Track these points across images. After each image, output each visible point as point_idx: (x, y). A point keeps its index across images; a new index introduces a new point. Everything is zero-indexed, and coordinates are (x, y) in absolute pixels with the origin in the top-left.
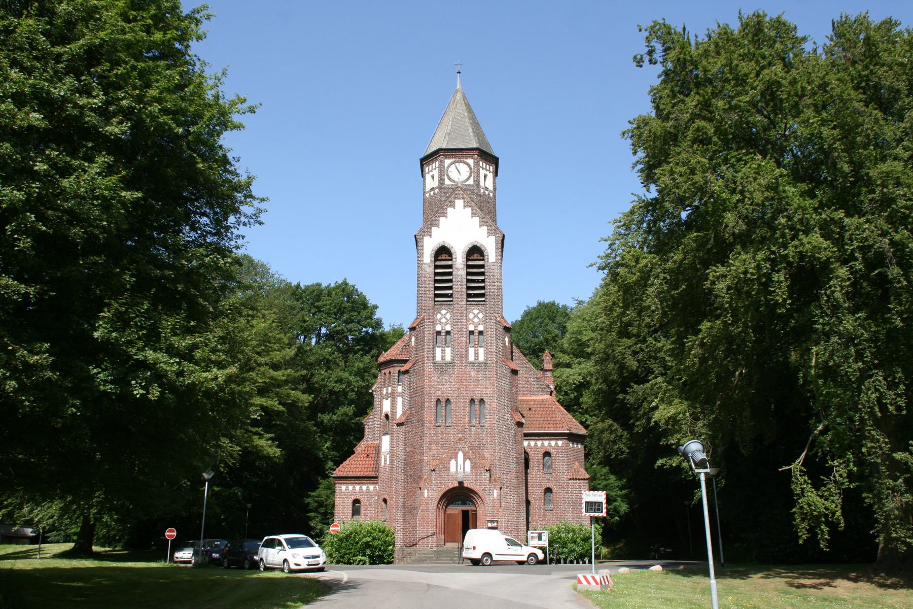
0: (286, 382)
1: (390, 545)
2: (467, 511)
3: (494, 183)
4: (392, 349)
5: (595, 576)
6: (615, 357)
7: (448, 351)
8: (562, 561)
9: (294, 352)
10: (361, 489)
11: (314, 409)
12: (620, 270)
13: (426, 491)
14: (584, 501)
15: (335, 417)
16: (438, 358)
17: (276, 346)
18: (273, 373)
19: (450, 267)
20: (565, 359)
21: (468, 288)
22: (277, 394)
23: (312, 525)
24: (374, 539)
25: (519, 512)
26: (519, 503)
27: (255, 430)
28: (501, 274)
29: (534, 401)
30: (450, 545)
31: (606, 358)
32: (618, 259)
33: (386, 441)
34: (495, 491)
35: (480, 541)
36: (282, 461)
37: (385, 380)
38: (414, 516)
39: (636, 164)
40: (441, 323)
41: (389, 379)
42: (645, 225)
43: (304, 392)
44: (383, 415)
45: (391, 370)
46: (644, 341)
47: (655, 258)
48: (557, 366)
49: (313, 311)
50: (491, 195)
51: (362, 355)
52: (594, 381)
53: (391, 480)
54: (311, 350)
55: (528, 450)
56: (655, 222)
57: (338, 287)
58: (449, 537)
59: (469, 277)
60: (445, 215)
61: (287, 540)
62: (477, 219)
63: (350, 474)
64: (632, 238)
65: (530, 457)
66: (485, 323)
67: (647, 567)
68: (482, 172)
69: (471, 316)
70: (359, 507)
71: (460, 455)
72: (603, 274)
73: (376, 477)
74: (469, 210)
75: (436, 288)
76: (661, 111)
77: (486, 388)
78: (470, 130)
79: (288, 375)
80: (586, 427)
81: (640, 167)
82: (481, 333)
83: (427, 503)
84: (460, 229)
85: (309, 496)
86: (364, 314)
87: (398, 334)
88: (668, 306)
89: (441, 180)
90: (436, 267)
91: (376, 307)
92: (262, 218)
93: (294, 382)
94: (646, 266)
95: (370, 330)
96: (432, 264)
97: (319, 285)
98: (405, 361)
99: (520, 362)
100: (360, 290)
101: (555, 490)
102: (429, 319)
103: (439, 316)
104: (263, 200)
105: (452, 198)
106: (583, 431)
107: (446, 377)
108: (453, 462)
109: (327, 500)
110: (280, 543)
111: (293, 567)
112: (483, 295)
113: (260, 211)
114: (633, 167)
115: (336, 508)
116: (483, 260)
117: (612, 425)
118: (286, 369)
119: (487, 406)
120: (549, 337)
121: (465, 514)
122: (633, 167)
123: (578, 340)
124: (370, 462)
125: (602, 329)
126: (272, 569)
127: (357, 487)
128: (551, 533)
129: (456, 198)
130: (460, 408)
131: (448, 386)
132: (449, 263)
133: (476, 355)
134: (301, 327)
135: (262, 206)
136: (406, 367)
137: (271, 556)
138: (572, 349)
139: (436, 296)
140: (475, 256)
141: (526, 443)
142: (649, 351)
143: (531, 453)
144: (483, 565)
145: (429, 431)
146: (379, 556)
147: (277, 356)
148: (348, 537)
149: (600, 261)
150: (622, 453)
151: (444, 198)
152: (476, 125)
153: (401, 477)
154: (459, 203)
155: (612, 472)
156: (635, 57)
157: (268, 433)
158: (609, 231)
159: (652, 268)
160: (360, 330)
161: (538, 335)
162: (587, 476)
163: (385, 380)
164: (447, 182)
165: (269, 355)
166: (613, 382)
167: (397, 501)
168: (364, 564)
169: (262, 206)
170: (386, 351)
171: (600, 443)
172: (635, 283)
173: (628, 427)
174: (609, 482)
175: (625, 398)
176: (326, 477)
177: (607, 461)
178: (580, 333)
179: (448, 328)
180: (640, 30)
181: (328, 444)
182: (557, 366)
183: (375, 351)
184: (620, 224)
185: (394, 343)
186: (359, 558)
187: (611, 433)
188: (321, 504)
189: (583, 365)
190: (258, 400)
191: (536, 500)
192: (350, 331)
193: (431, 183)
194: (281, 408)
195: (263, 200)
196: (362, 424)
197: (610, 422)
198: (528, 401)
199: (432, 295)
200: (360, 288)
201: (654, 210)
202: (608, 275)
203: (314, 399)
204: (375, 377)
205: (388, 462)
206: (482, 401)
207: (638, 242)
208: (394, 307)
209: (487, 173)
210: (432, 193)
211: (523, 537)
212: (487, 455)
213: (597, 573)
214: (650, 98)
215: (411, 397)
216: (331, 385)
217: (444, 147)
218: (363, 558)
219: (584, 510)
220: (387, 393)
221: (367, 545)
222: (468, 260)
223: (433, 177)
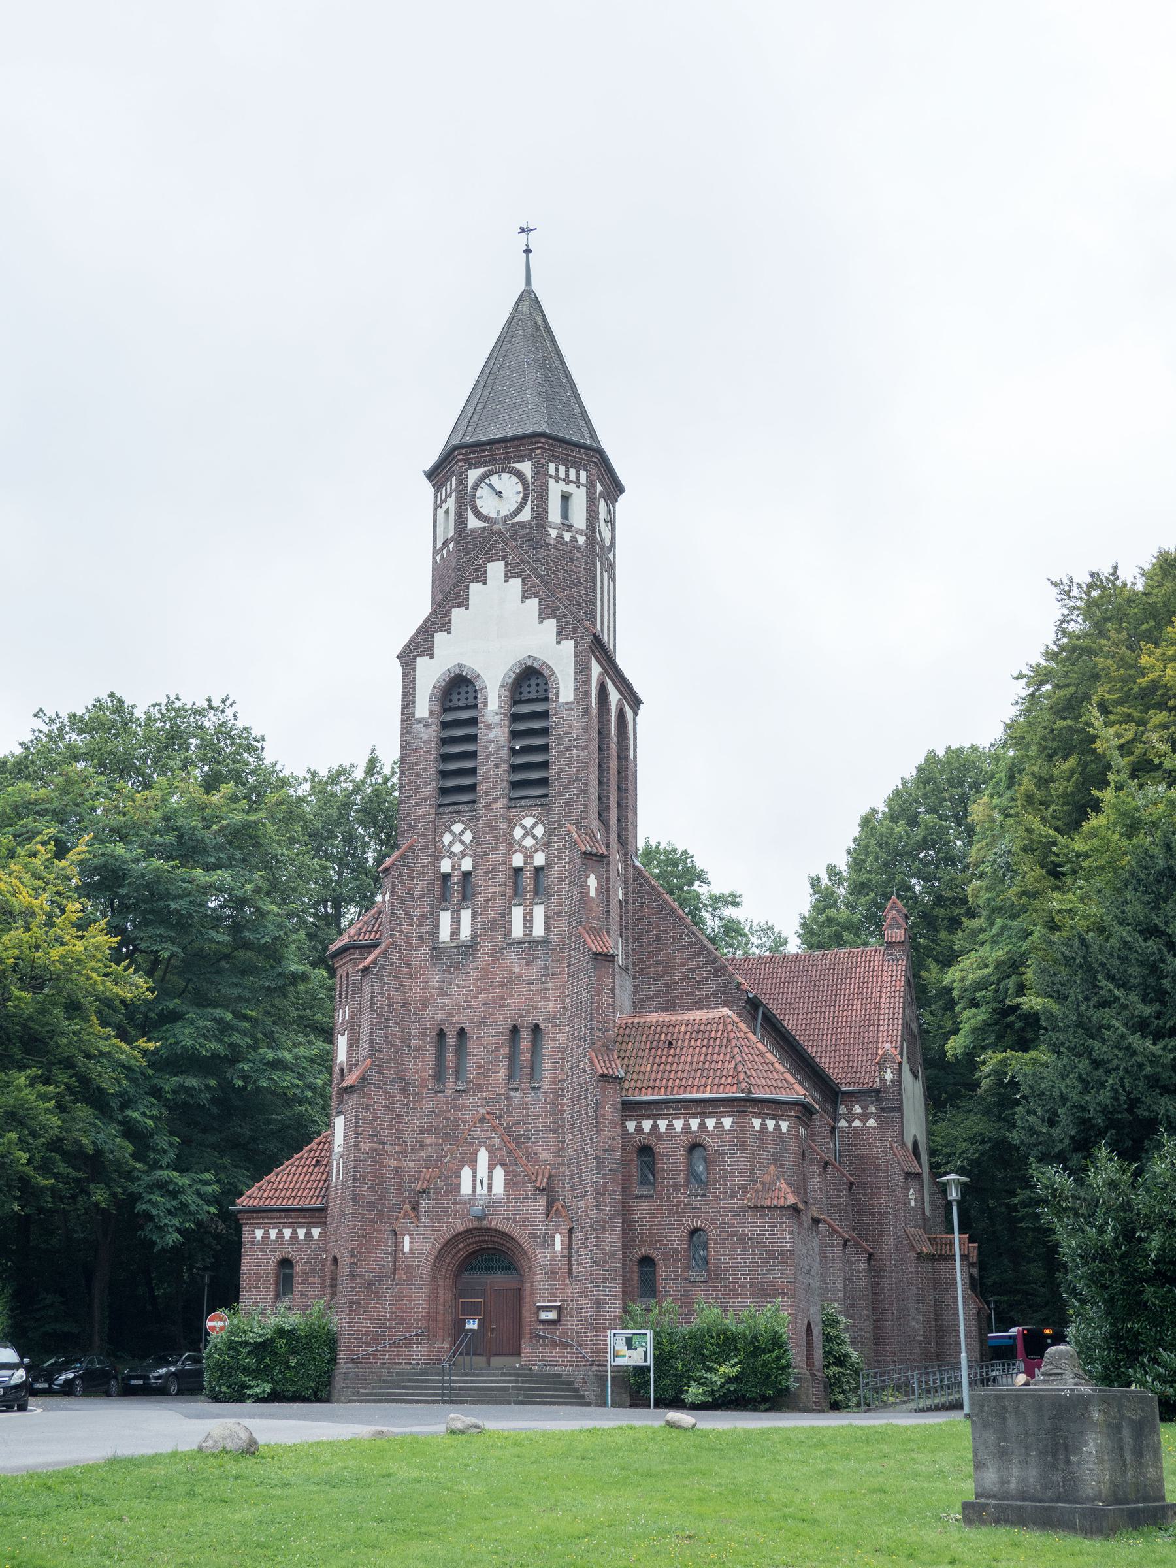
10: (294, 1235)
13: (407, 1239)
16: (445, 935)
34: (558, 1237)
40: (452, 855)
50: (581, 540)
62: (534, 603)
63: (272, 1204)
66: (546, 847)
71: (483, 1156)
73: (324, 1210)
83: (409, 1266)
89: (461, 520)
96: (434, 720)
107: (458, 979)
108: (466, 1173)
112: (544, 782)
130: (488, 1053)
131: (461, 998)
154: (496, 569)
164: (473, 523)
198: (670, 1024)
206: (536, 1029)
209: (571, 488)
210: (445, 552)
212: (544, 1155)
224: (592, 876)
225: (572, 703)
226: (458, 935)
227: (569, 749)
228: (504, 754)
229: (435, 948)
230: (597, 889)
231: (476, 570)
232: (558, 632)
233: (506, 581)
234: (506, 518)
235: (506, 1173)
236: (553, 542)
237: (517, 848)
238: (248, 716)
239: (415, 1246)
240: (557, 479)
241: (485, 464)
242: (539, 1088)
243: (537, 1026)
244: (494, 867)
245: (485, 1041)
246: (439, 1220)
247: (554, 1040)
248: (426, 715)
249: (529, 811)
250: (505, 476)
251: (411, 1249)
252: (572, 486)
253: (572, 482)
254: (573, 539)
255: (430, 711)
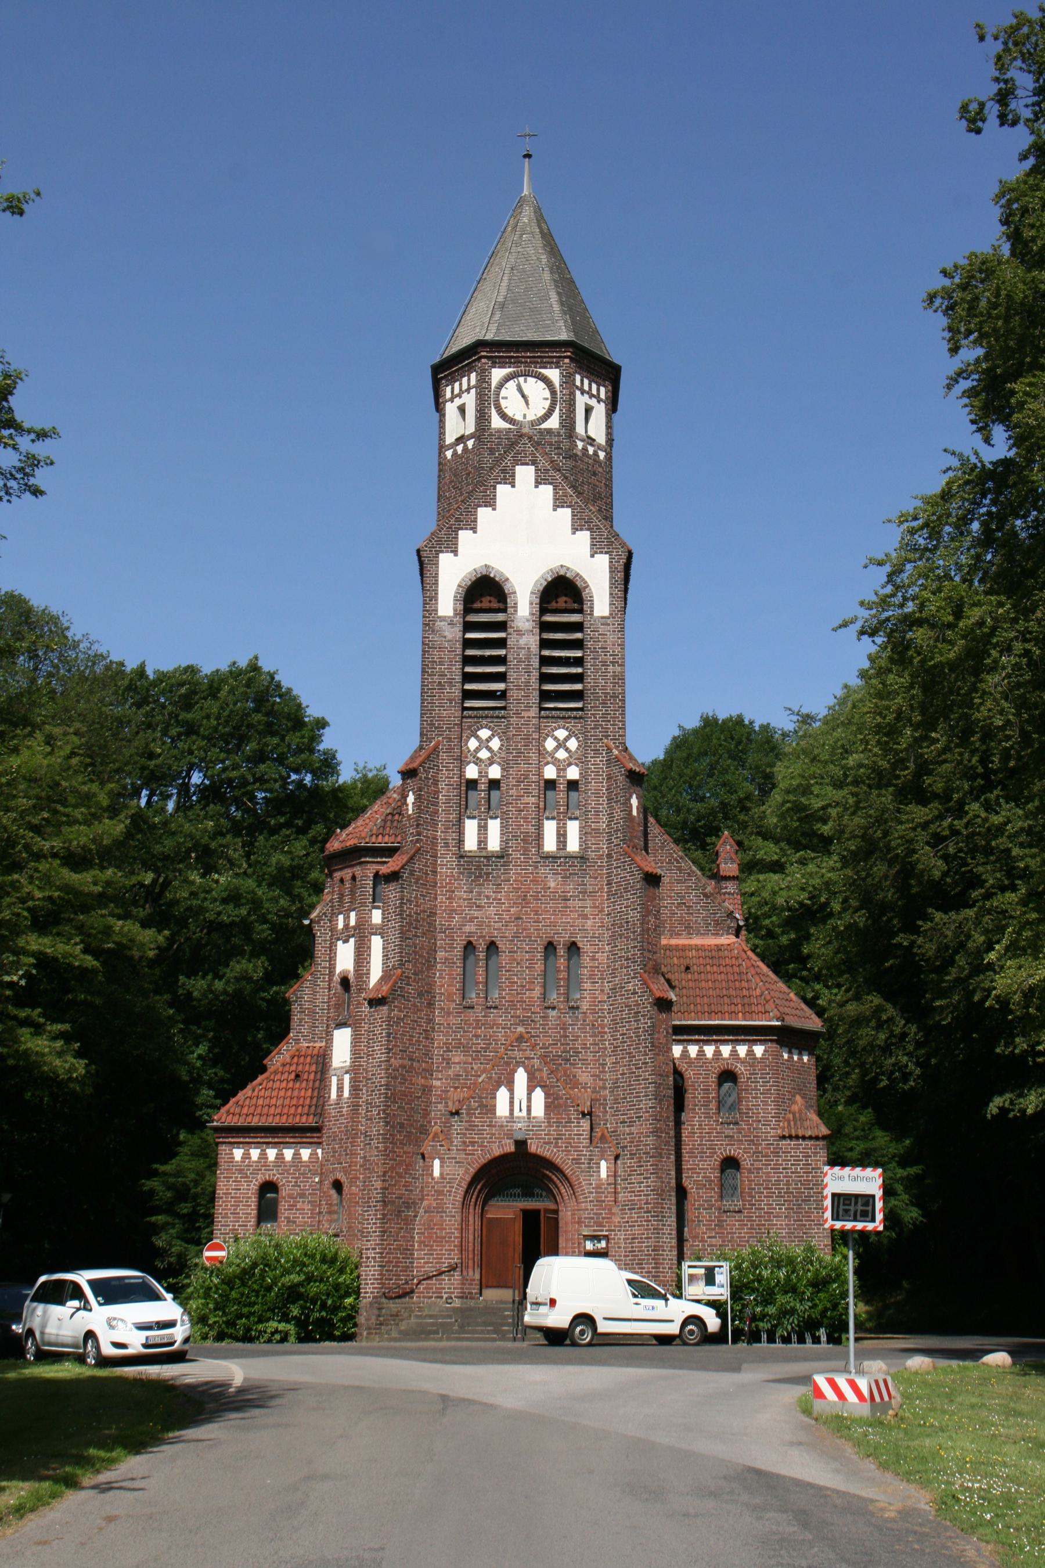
0: (102, 899)
1: (347, 1295)
2: (537, 1212)
3: (609, 426)
4: (360, 822)
5: (854, 1379)
6: (889, 849)
7: (494, 826)
8: (764, 1337)
9: (121, 827)
10: (280, 1156)
11: (172, 963)
12: (919, 635)
13: (437, 1163)
14: (828, 1192)
15: (219, 985)
16: (471, 843)
17: (78, 813)
18: (74, 878)
19: (502, 626)
20: (768, 851)
21: (544, 678)
22: (80, 928)
23: (160, 1243)
24: (461, 391)
25: (660, 1216)
26: (660, 1193)
27: (22, 1014)
28: (622, 645)
29: (697, 948)
30: (491, 1294)
31: (869, 849)
32: (910, 607)
33: (342, 1042)
34: (603, 1164)
35: (571, 1284)
36: (89, 1090)
37: (341, 896)
38: (409, 1222)
39: (954, 380)
40: (478, 761)
41: (353, 892)
42: (975, 526)
43: (145, 924)
44: (336, 978)
45: (358, 870)
46: (959, 811)
47: (1001, 604)
48: (750, 867)
49: (174, 732)
50: (602, 455)
51: (286, 840)
52: (836, 906)
53: (352, 1135)
54: (165, 823)
55: (683, 1067)
56: (1001, 519)
57: (235, 673)
58: (492, 1277)
59: (546, 653)
60: (490, 502)
61: (96, 1285)
62: (566, 513)
63: (255, 1122)
64: (943, 557)
65: (688, 1083)
67: (975, 1354)
68: (581, 400)
69: (550, 744)
70: (275, 1203)
71: (521, 1077)
72: (869, 646)
73: (318, 1129)
74: (547, 490)
75: (468, 678)
76: (1026, 244)
77: (585, 917)
78: (554, 297)
79: (108, 883)
80: (820, 1013)
81: (965, 384)
82: (573, 785)
83: (440, 1193)
84: (526, 535)
85: (155, 1173)
86: (294, 739)
87: (374, 788)
88: (1030, 721)
89: (482, 417)
90: (468, 627)
91: (322, 724)
92: (41, 478)
93: (120, 901)
94: (981, 624)
95: (308, 779)
96: (459, 620)
97: (191, 670)
98: (391, 852)
99: (666, 856)
100: (285, 684)
101: (746, 1162)
102: (450, 749)
103: (473, 744)
104: (42, 435)
105: (508, 461)
106: (814, 1023)
107: (489, 890)
108: (502, 1094)
109: (196, 1183)
110: (77, 1292)
111: (108, 1350)
112: (578, 696)
113: (33, 462)
114: (949, 387)
115: (219, 1202)
116: (580, 611)
117: (879, 1009)
118: (102, 868)
119: (586, 960)
120: (733, 799)
121: (531, 1219)
122: (949, 387)
123: (798, 808)
124: (304, 1092)
125: (856, 783)
126: (57, 1357)
127: (272, 1153)
128: (738, 1267)
129: (517, 462)
130: (521, 965)
132: (500, 617)
133: (562, 837)
134: (143, 768)
135: (41, 449)
136: (392, 864)
137: (58, 1322)
138: (785, 827)
139: (468, 695)
140: (562, 602)
141: (677, 1050)
142: (974, 834)
143: (689, 1074)
144: (574, 1344)
145: (446, 1018)
146: (321, 1322)
147: (80, 836)
148: (246, 1274)
149: (865, 614)
150: (906, 1077)
151: (488, 460)
152: (567, 287)
153: (377, 1129)
154: (525, 474)
155: (882, 1122)
156: (964, 108)
157: (54, 1021)
158: (890, 541)
159: (994, 629)
160: (284, 779)
161: (706, 791)
162: (824, 1131)
163: (341, 896)
164: (497, 422)
165: (58, 833)
166: (884, 907)
167: (367, 1187)
168: (284, 1339)
169: (41, 449)
170: (343, 827)
171: (853, 1053)
172: (953, 666)
173: (917, 1012)
174: (874, 1144)
175: (913, 943)
176: (198, 1125)
177: (868, 1095)
178: (806, 791)
179: (495, 772)
180: (982, 38)
181: (202, 1049)
182: (750, 867)
183: (319, 828)
184: (915, 524)
185: (364, 809)
186: (273, 1325)
187: (879, 1027)
188: (182, 1194)
189: (811, 867)
190: (35, 942)
191: (700, 1186)
192: (261, 780)
193: (457, 425)
194: (90, 961)
195: (42, 435)
196: (287, 1002)
197: (877, 1000)
198: (684, 948)
199: (458, 694)
200: (286, 680)
201: (998, 491)
202: (883, 648)
203: (171, 940)
204: (318, 889)
205: (346, 1094)
206: (573, 948)
207: (959, 567)
208: (367, 725)
209: (593, 402)
210: (460, 449)
211: (670, 1276)
212: (584, 1077)
213: (860, 1372)
214: (997, 212)
215: (403, 936)
216: (214, 909)
217: (489, 337)
218: (282, 1326)
219: (828, 1214)
220: (346, 926)
221: (293, 1294)
222: (543, 611)
223: (462, 409)
224: (634, 796)
225: (608, 618)
226: (486, 844)
227: (605, 664)
228: (535, 662)
229: (462, 857)
230: (638, 808)
231: (504, 471)
232: (592, 545)
233: (537, 487)
234: (533, 423)
235: (547, 1095)
236: (579, 453)
237: (549, 759)
238: (27, 596)
239: (447, 1170)
240: (583, 392)
241: (510, 365)
242: (578, 1008)
243: (574, 944)
244: (526, 777)
245: (518, 956)
246: (473, 1143)
247: (593, 959)
248: (451, 613)
249: (561, 722)
250: (531, 380)
251: (441, 1174)
252: (594, 400)
253: (594, 396)
254: (596, 454)
255: (455, 610)
